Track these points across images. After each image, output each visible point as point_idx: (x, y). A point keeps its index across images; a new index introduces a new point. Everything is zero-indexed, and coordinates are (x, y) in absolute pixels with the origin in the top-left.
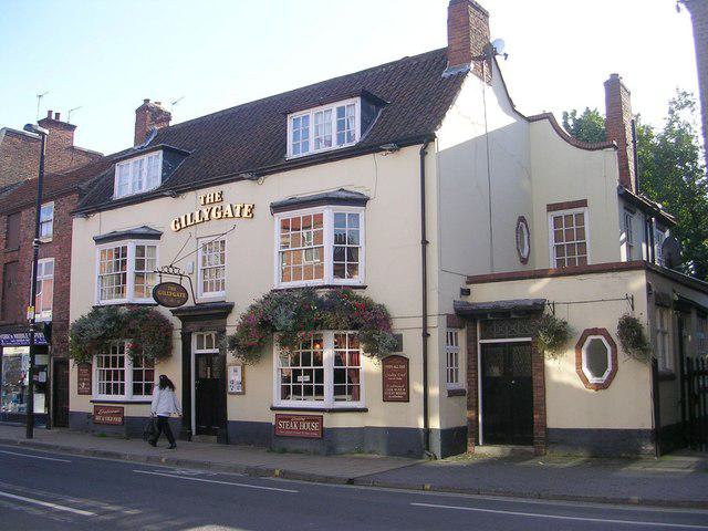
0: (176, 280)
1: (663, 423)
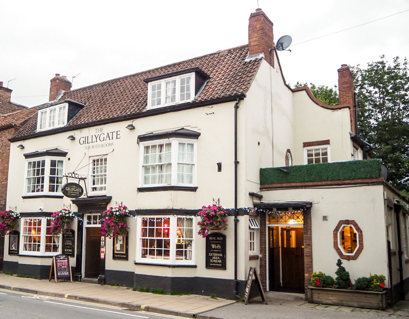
0: (76, 181)
1: (394, 283)
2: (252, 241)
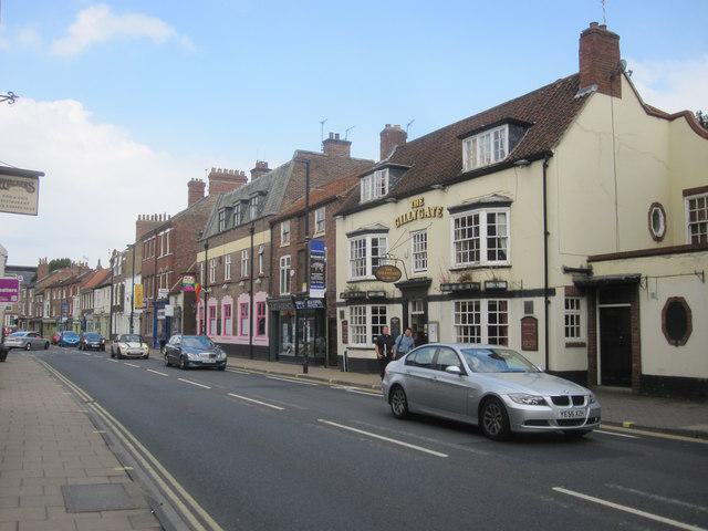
2: (570, 326)
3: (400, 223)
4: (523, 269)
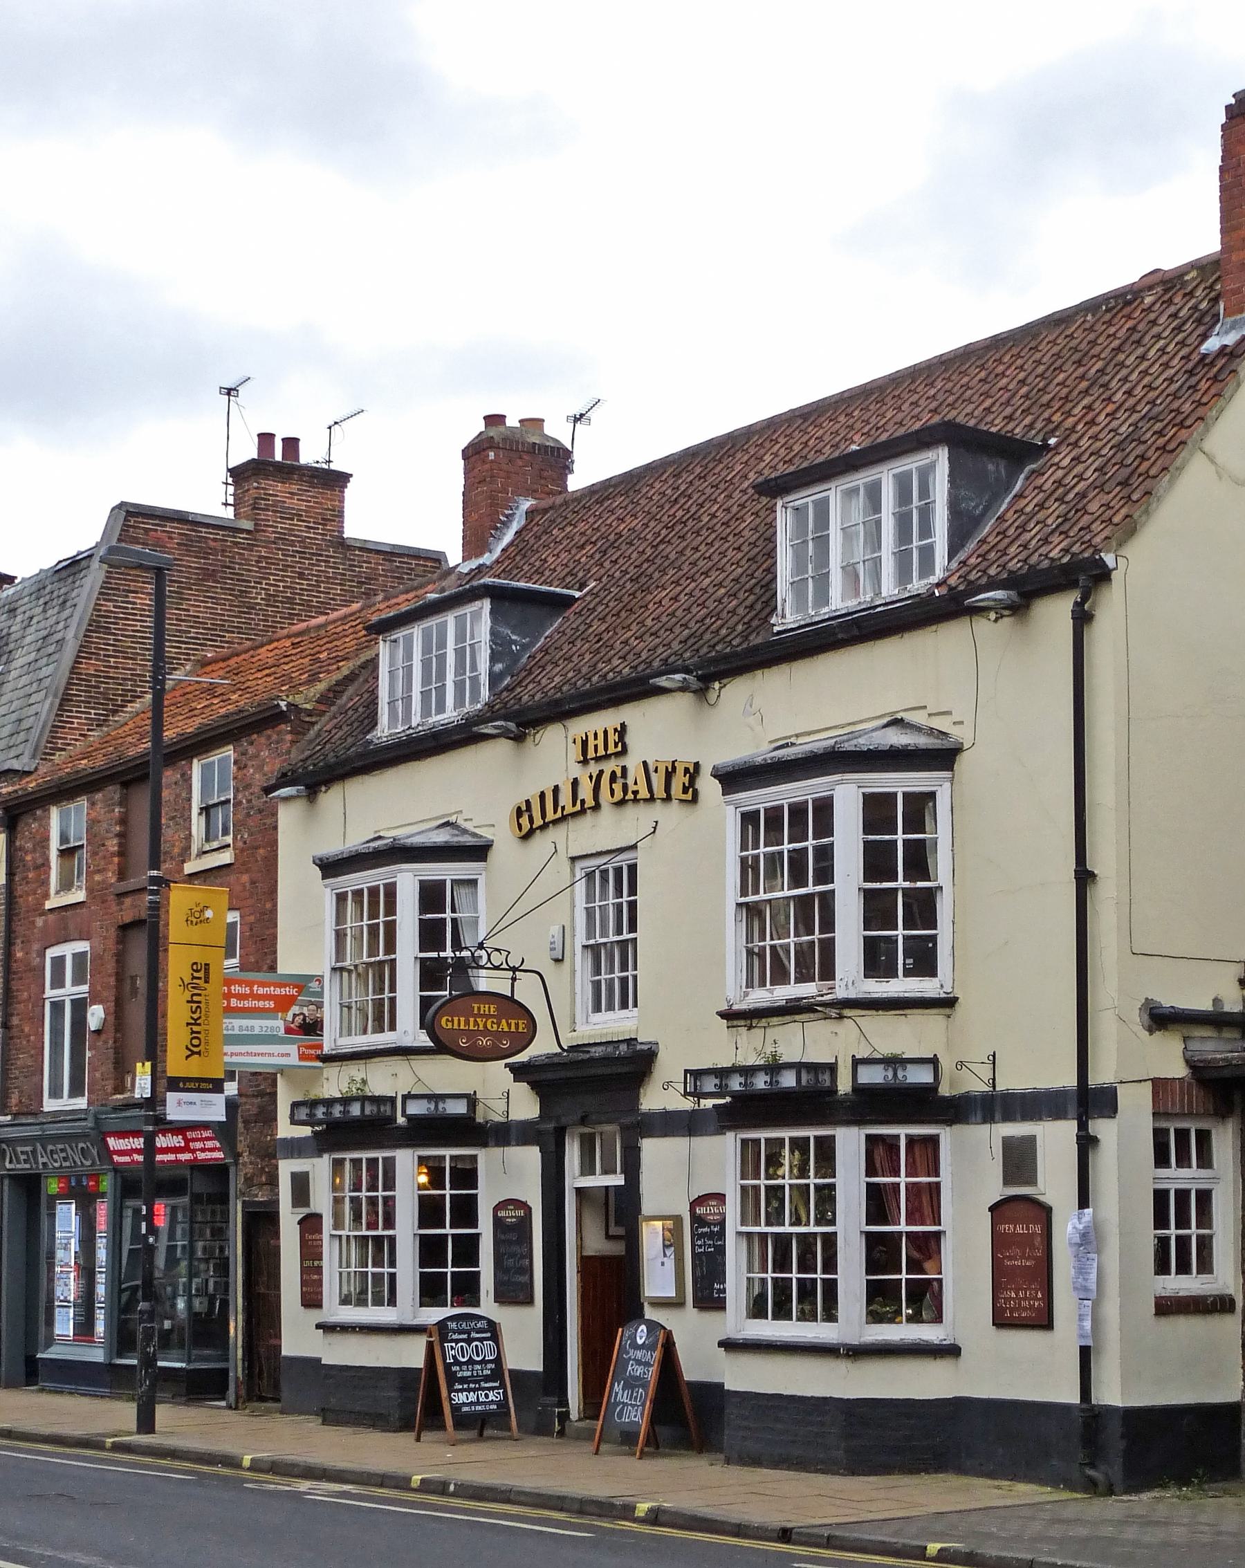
2: (1173, 1232)
3: (532, 820)
4: (1001, 1010)
